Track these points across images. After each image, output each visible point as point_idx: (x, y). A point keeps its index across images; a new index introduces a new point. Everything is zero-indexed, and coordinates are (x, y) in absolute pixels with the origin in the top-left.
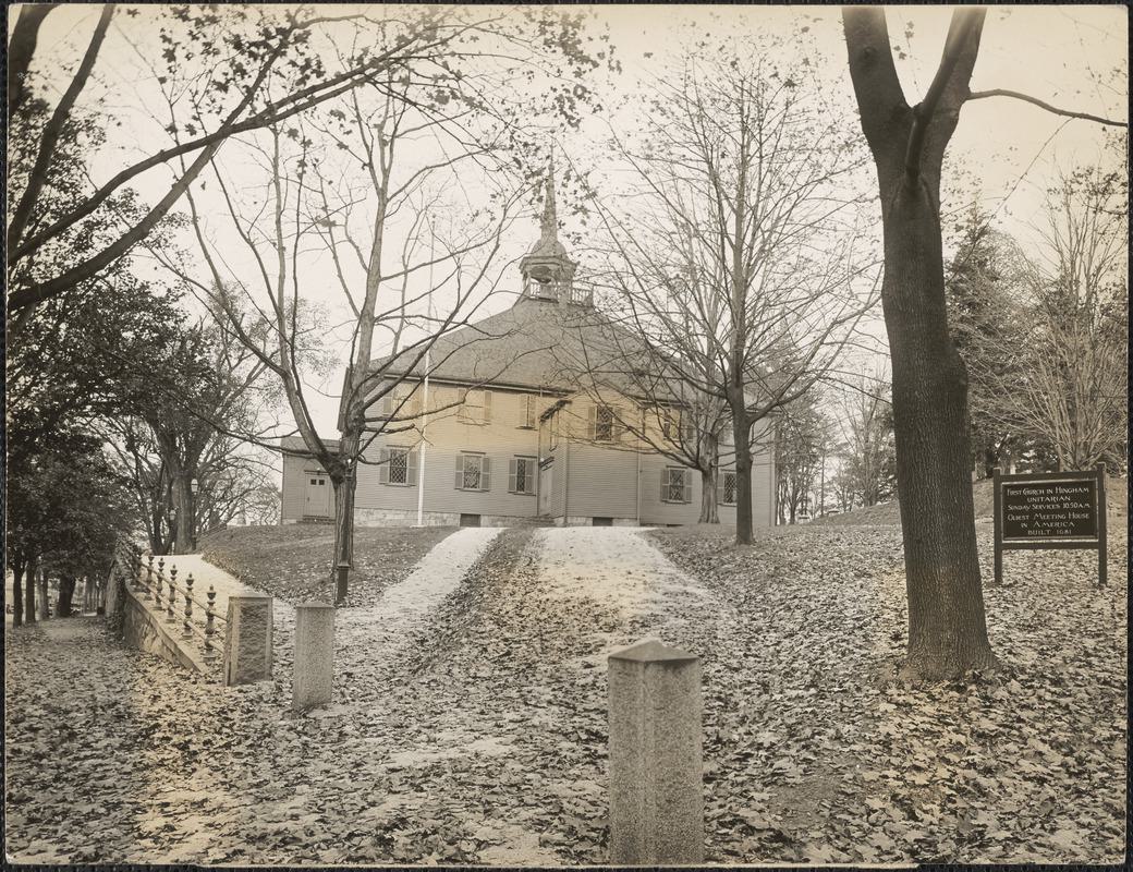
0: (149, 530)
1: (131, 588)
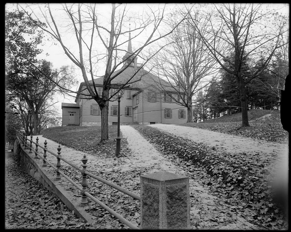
0: (25, 130)
1: (23, 148)
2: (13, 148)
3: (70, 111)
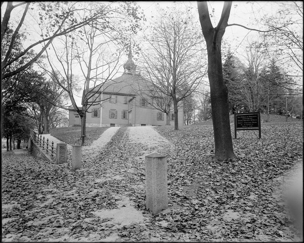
0: (38, 129)
2: (28, 145)
3: (75, 114)
